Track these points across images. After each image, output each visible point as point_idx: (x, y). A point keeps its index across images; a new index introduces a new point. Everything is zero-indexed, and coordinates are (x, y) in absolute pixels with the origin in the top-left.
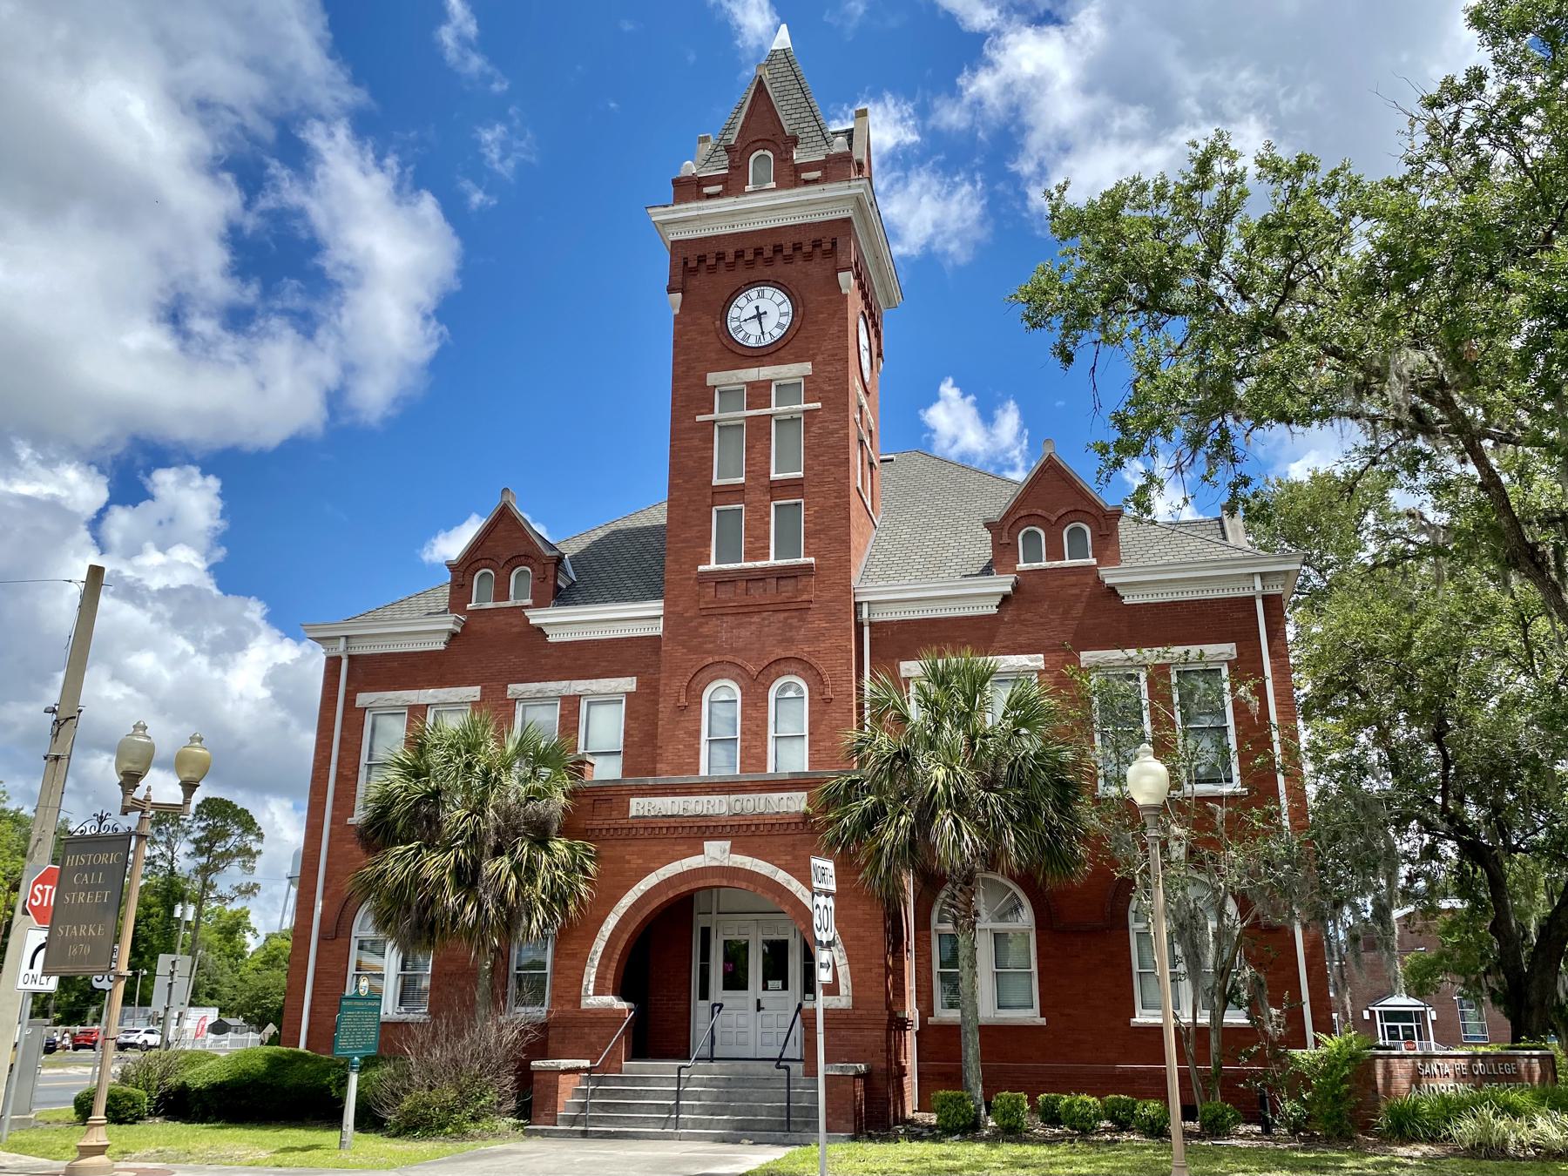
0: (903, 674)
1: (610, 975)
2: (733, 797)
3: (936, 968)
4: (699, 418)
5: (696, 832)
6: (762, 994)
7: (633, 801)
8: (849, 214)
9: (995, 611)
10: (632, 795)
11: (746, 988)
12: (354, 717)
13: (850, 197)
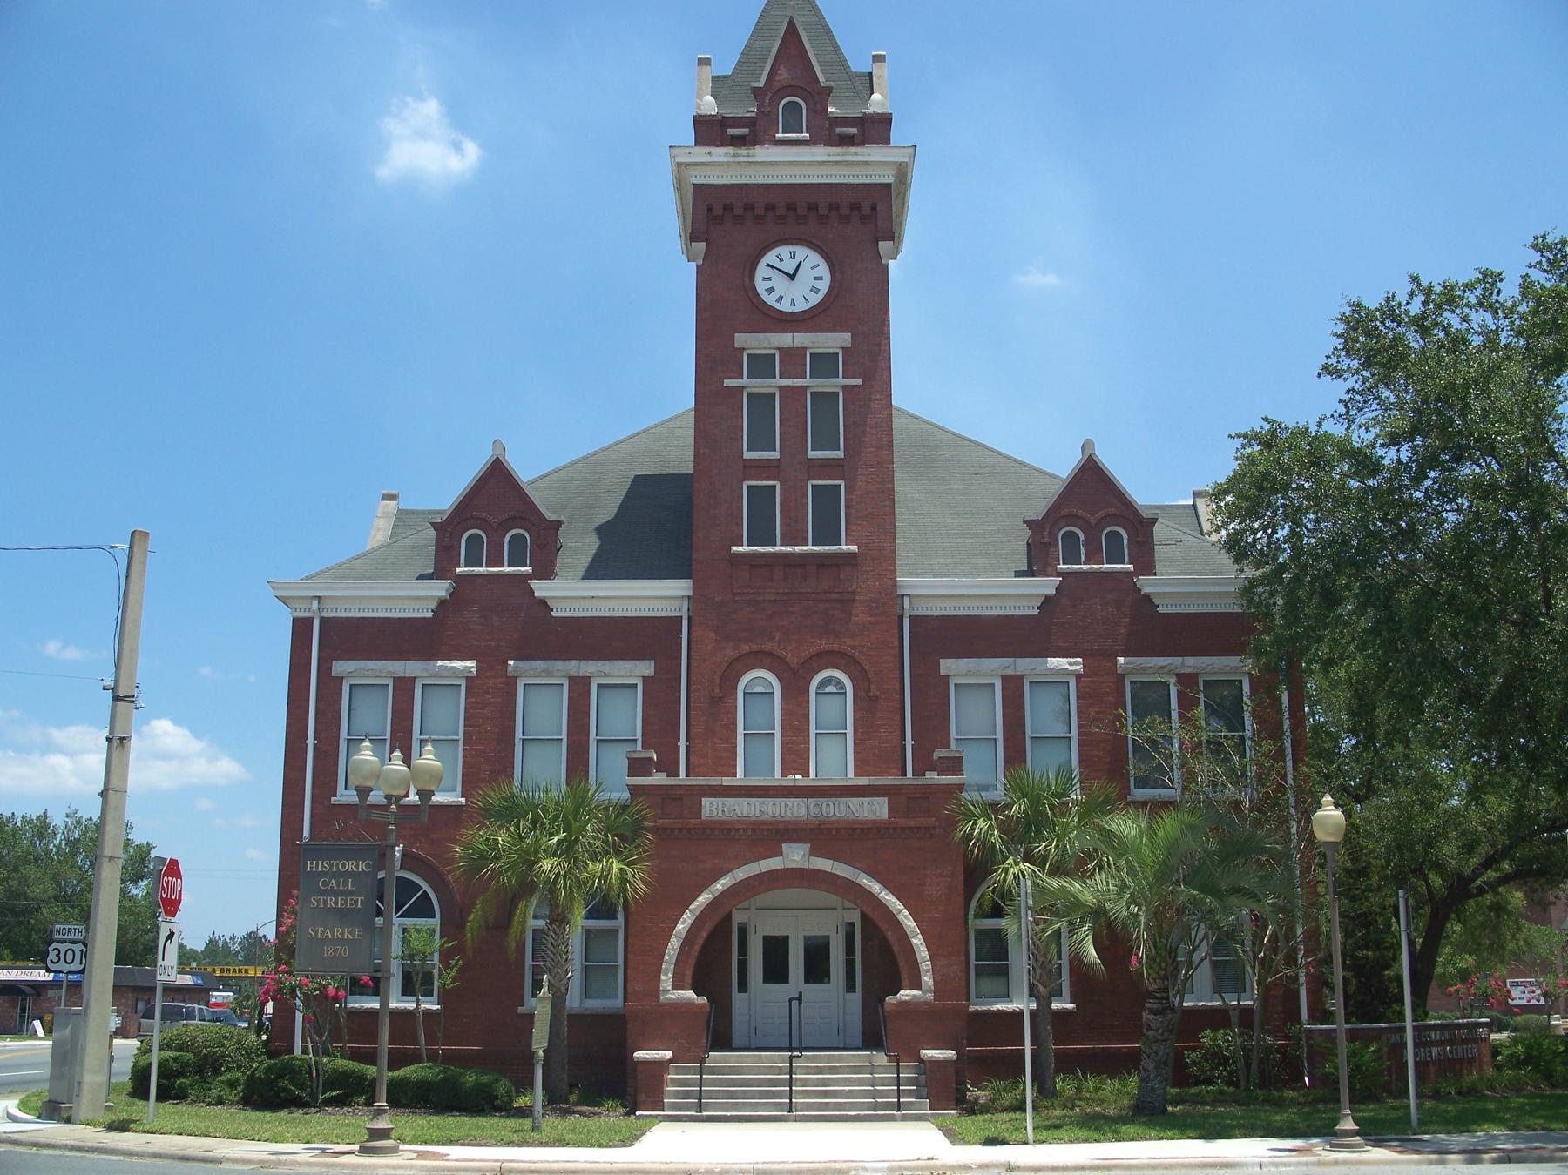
3: (973, 962)
4: (727, 383)
6: (803, 987)
7: (706, 802)
8: (891, 180)
11: (807, 981)
13: (895, 163)
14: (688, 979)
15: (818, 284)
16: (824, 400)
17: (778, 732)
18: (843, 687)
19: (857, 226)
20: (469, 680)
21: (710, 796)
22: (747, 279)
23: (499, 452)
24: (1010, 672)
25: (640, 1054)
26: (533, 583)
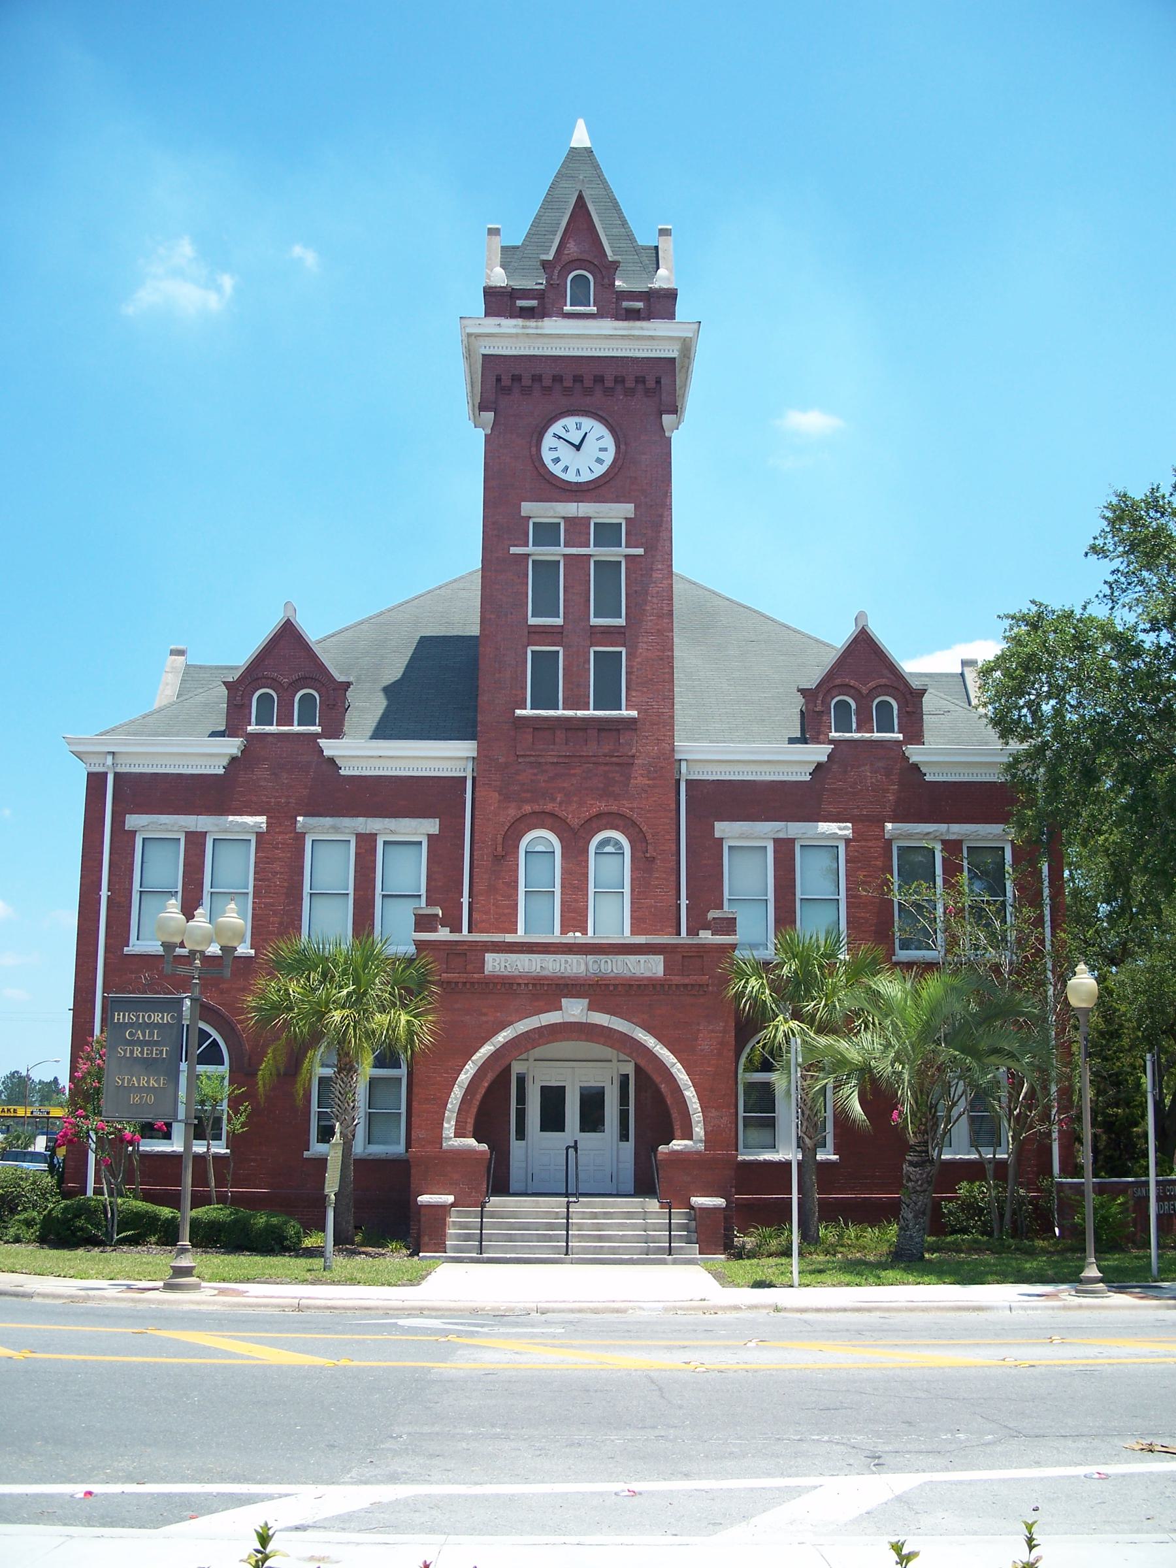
0: (717, 835)
1: (471, 1121)
3: (741, 1113)
4: (513, 550)
7: (489, 957)
8: (675, 354)
9: (808, 778)
10: (488, 951)
12: (124, 839)
13: (679, 338)
14: (470, 1128)
15: (602, 455)
16: (608, 568)
18: (621, 848)
19: (641, 397)
21: (493, 951)
22: (534, 449)
23: (290, 614)
24: (782, 835)
25: (424, 1199)
26: (322, 742)
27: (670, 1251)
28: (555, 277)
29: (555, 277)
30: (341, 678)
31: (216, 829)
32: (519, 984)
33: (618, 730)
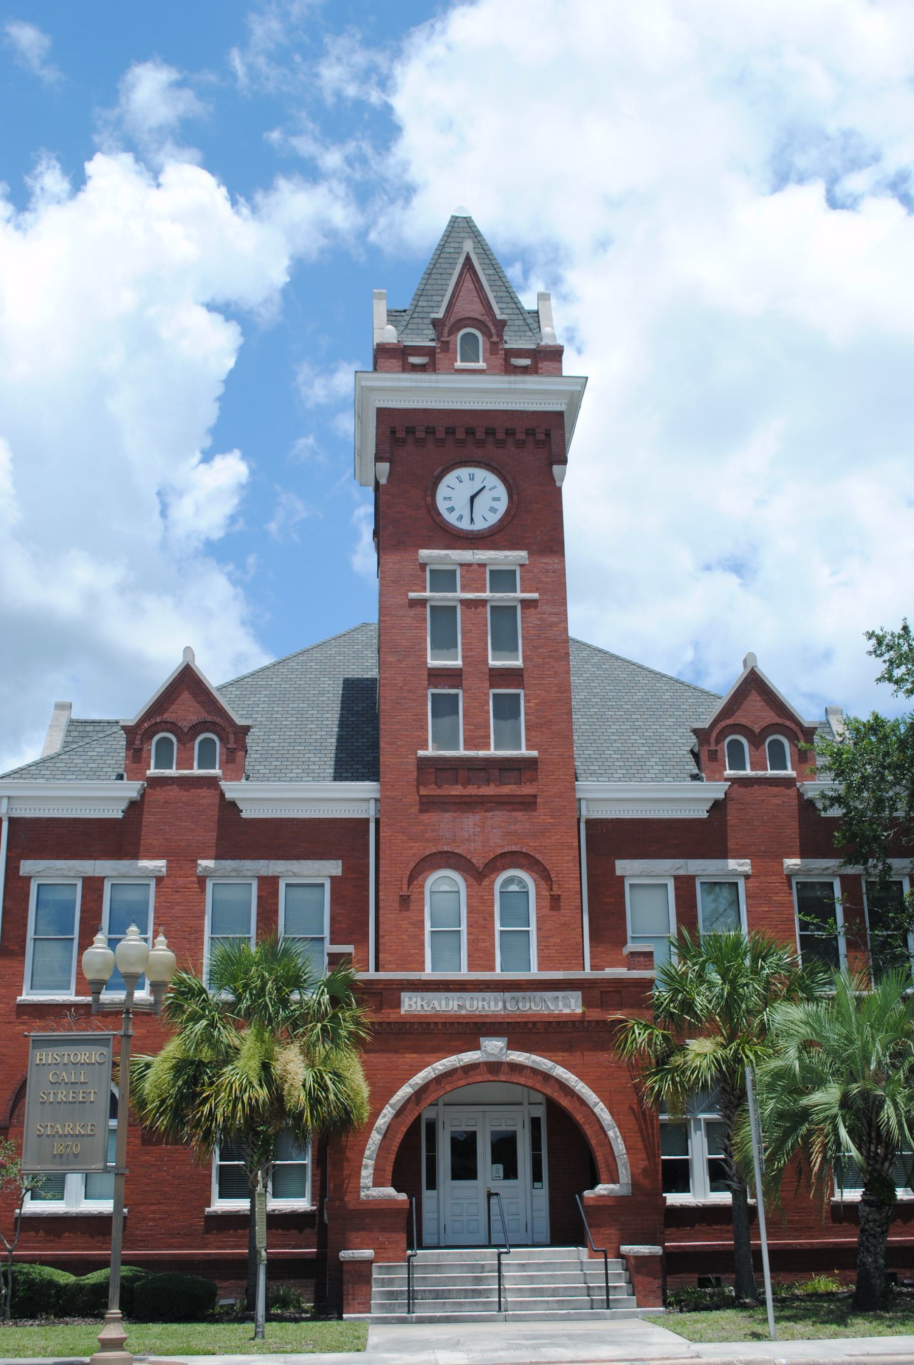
0: (618, 872)
1: (389, 1168)
2: (507, 994)
5: (469, 1032)
15: (495, 504)
16: (503, 613)
17: (464, 928)
19: (531, 449)
20: (159, 880)
22: (429, 499)
23: (189, 659)
24: (681, 872)
25: (345, 1255)
26: (224, 785)
27: (608, 1304)
28: (445, 334)
29: (445, 334)
30: (240, 722)
31: (115, 874)
32: (437, 1023)
33: (519, 769)
